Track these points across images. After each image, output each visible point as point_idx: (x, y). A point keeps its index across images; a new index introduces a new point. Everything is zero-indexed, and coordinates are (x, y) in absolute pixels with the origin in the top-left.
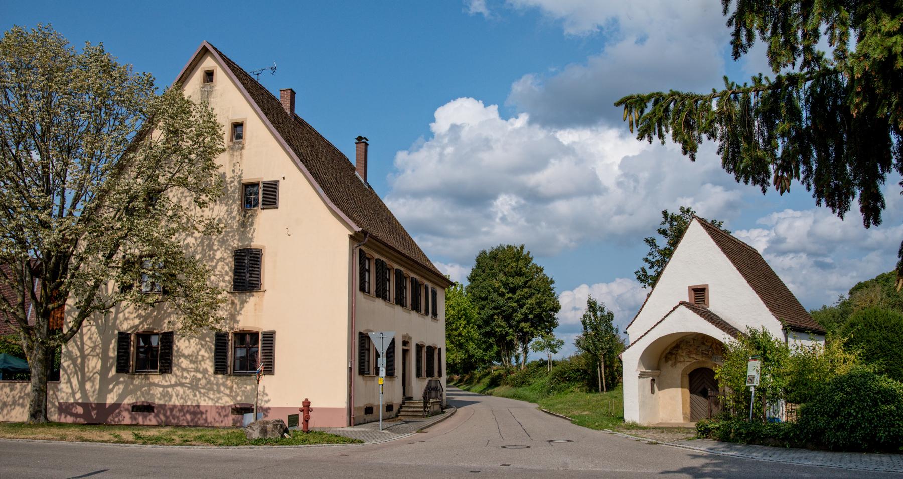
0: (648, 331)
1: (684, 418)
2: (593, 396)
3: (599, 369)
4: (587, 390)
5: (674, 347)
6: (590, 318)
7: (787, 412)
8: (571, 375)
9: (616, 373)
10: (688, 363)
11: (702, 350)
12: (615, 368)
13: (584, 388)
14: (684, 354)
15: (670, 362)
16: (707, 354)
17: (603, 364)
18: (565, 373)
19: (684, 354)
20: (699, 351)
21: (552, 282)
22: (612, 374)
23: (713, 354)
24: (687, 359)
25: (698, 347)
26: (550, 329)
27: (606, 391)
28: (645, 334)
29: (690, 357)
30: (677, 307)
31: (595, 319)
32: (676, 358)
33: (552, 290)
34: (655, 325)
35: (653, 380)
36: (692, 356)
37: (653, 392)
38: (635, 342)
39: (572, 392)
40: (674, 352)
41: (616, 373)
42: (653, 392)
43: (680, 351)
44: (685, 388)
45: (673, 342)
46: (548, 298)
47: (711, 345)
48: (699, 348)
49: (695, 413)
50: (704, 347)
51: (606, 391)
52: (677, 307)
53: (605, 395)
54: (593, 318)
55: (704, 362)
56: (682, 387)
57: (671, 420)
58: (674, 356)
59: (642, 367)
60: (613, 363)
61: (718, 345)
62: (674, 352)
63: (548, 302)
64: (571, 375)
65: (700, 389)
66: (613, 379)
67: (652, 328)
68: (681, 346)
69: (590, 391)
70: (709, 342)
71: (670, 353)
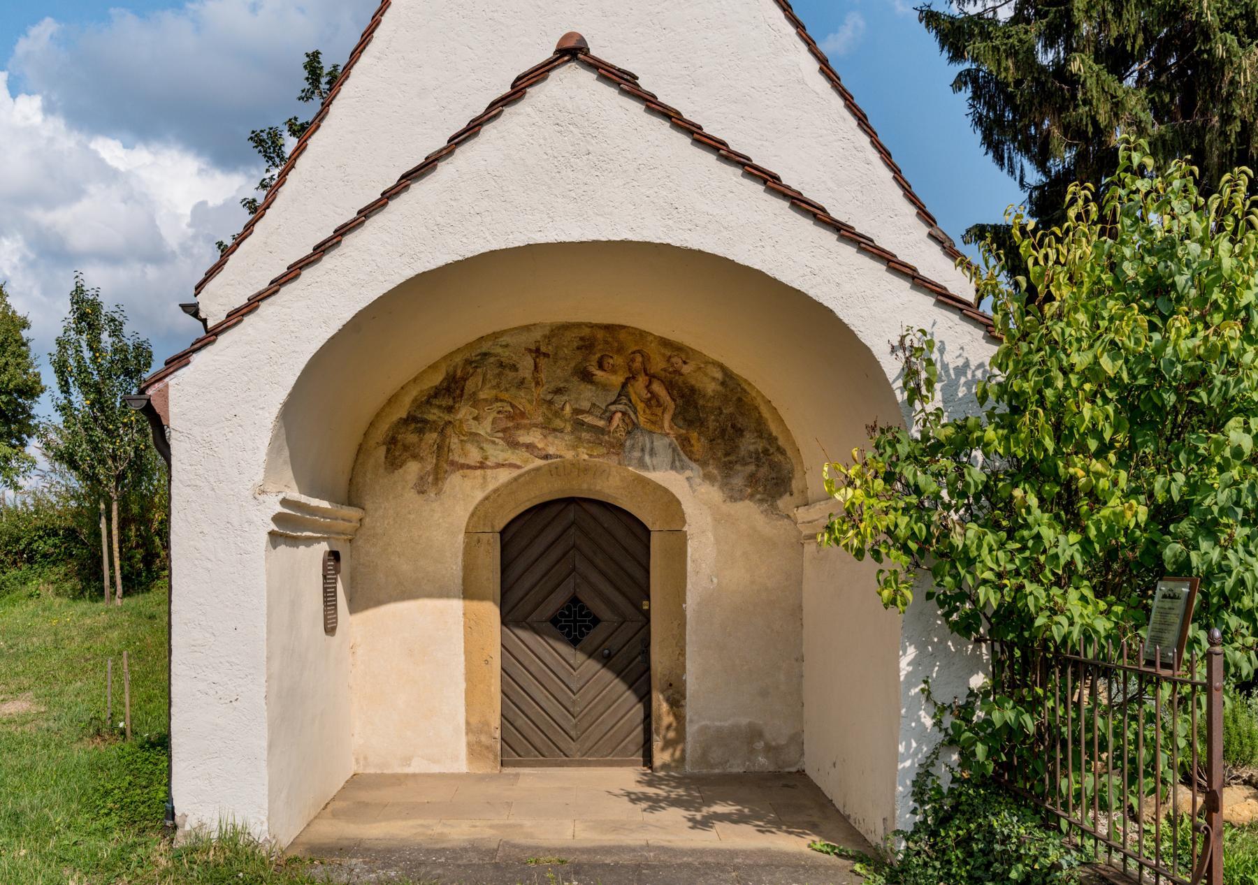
0: (342, 231)
1: (474, 751)
2: (84, 614)
3: (103, 525)
4: (73, 589)
5: (437, 393)
6: (78, 351)
7: (129, 540)
8: (35, 546)
9: (157, 539)
10: (504, 476)
11: (577, 411)
12: (156, 525)
13: (68, 586)
14: (484, 428)
15: (413, 469)
16: (601, 431)
17: (115, 507)
18: (18, 540)
19: (484, 428)
20: (557, 414)
21: (25, 324)
22: (145, 542)
23: (632, 428)
24: (498, 453)
25: (558, 391)
26: (20, 439)
27: (126, 593)
28: (322, 249)
29: (514, 445)
30: (538, 74)
31: (94, 360)
32: (441, 449)
33: (24, 344)
34: (389, 195)
35: (334, 555)
36: (524, 438)
37: (330, 629)
38: (253, 304)
39: (31, 596)
40: (434, 415)
41: (157, 539)
42: (330, 629)
43: (464, 412)
44: (481, 598)
45: (434, 367)
46: (12, 361)
47: (624, 385)
48: (559, 400)
49: (521, 721)
50: (586, 396)
51: (126, 593)
52: (538, 74)
53: (120, 610)
54: (87, 354)
55: (584, 469)
56: (469, 592)
57: (407, 760)
58: (431, 437)
59: (288, 474)
60: (149, 511)
61: (657, 387)
62: (434, 415)
63: (11, 369)
64: (35, 546)
65: (557, 601)
66: (150, 558)
67: (367, 213)
68: (470, 385)
69: (78, 595)
70: (614, 371)
71: (414, 421)
